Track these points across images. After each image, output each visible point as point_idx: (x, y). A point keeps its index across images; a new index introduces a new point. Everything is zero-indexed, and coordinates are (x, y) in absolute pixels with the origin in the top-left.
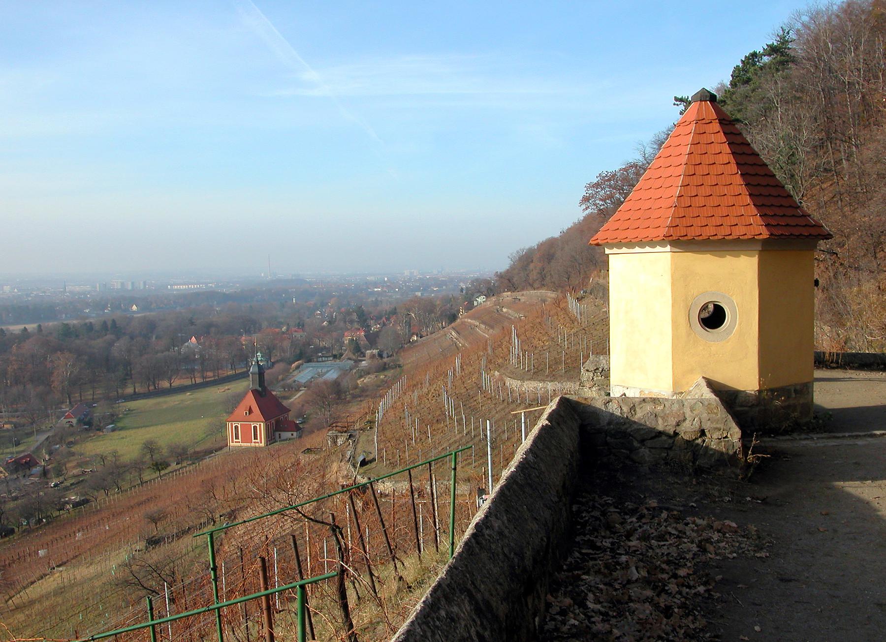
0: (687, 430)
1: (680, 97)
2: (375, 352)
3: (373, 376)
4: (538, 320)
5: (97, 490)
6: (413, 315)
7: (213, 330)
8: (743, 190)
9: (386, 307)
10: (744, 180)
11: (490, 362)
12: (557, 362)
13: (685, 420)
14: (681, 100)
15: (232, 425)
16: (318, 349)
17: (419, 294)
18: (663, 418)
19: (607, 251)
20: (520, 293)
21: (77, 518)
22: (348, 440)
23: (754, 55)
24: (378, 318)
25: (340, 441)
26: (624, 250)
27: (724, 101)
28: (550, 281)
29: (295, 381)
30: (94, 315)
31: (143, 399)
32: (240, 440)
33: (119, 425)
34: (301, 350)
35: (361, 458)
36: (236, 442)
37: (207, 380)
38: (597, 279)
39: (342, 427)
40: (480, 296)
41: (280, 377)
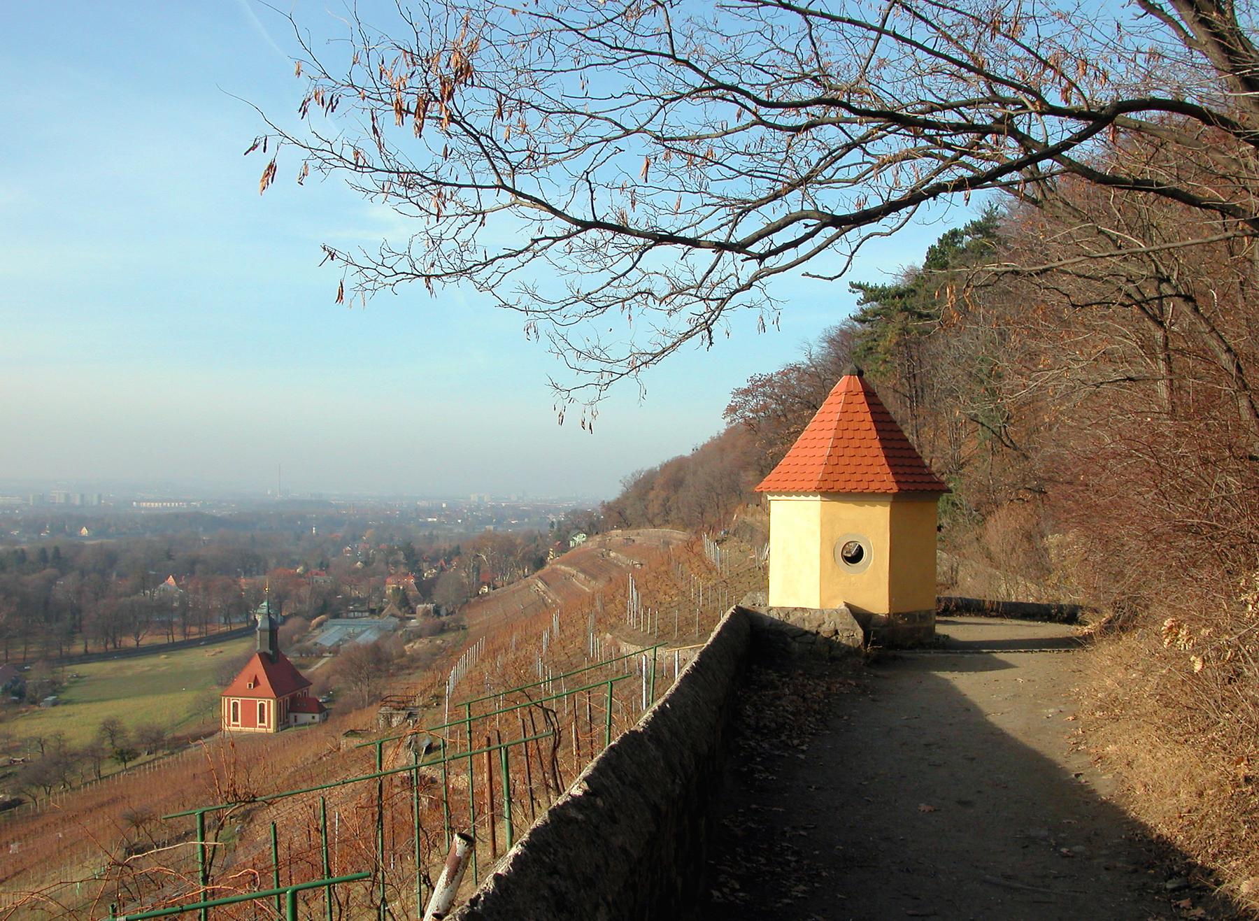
0: (826, 630)
1: (858, 283)
2: (430, 606)
3: (426, 641)
4: (663, 568)
5: (37, 786)
6: (484, 557)
7: (198, 567)
8: (881, 452)
9: (444, 545)
10: (881, 444)
11: (599, 621)
12: (689, 623)
13: (824, 623)
14: (859, 287)
16: (348, 600)
17: (491, 527)
18: (809, 622)
19: (769, 498)
20: (635, 532)
21: (8, 824)
22: (406, 719)
23: (954, 233)
24: (433, 560)
25: (395, 721)
26: (783, 497)
27: (912, 291)
28: (676, 517)
29: (316, 644)
30: (24, 539)
31: (98, 661)
32: (239, 723)
33: (64, 697)
34: (325, 601)
35: (427, 742)
36: (233, 725)
37: (191, 637)
38: (742, 516)
39: (398, 703)
40: (578, 534)
41: (295, 638)
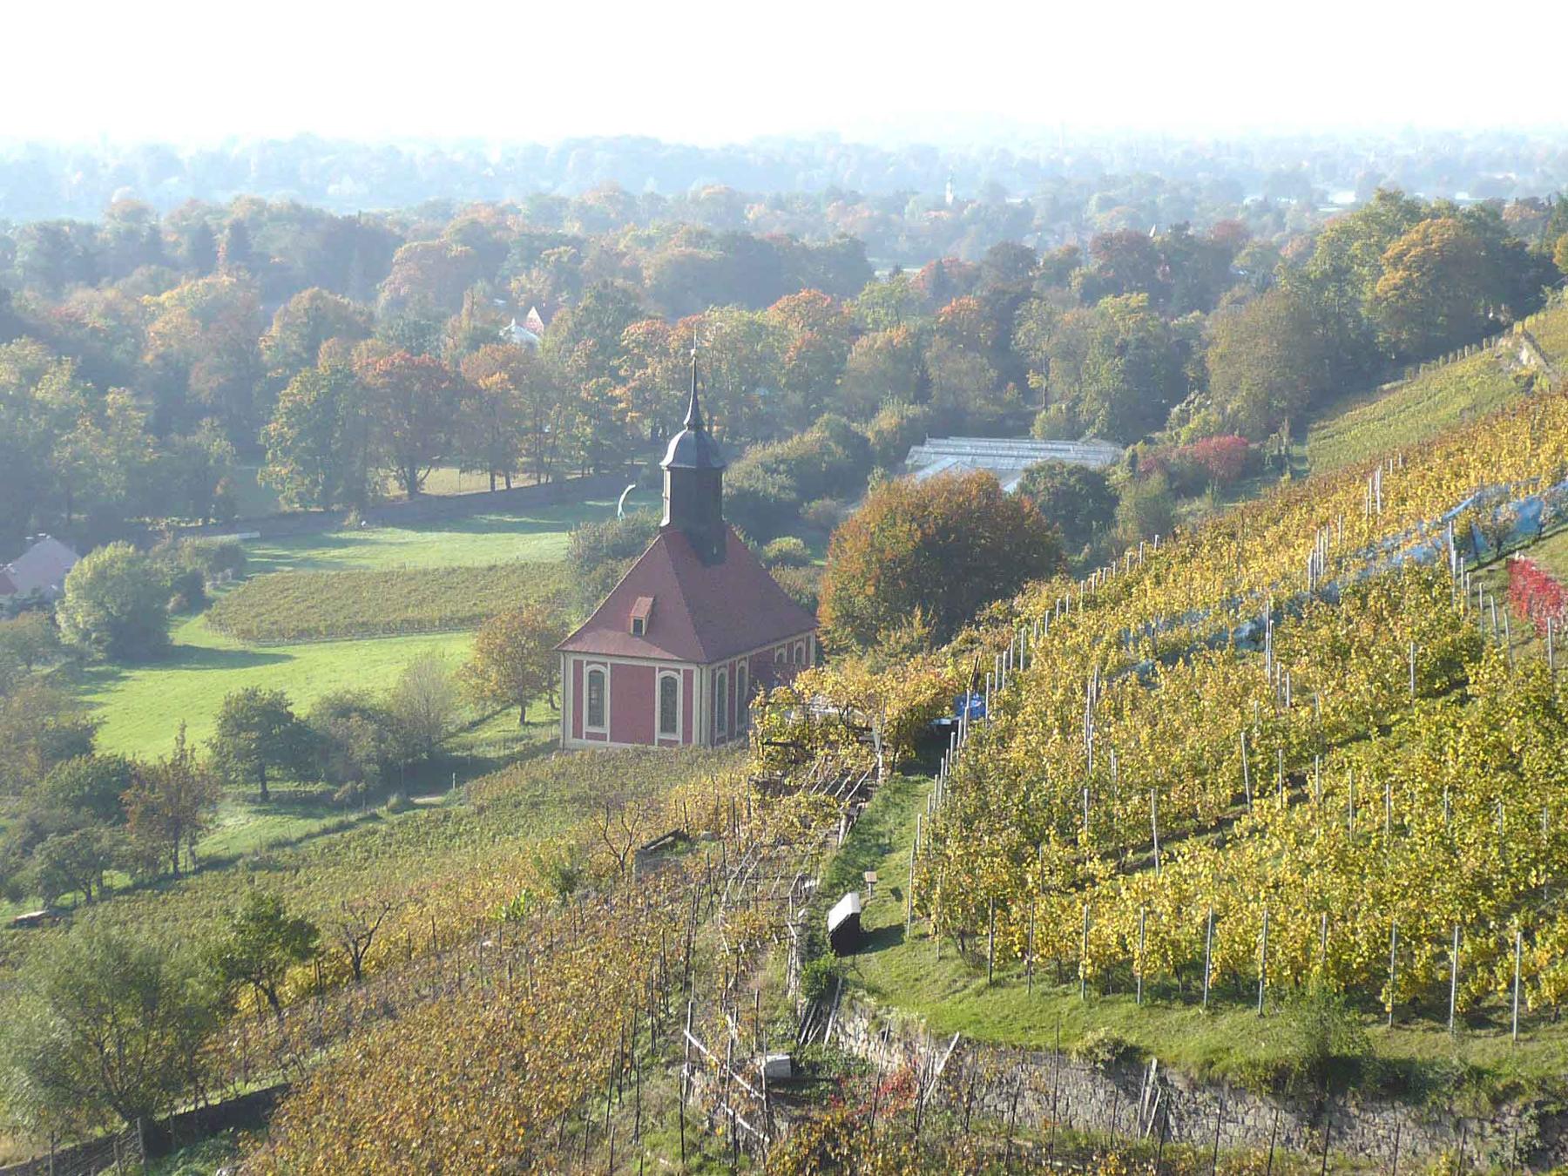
15: (578, 666)
32: (606, 729)
36: (591, 736)
